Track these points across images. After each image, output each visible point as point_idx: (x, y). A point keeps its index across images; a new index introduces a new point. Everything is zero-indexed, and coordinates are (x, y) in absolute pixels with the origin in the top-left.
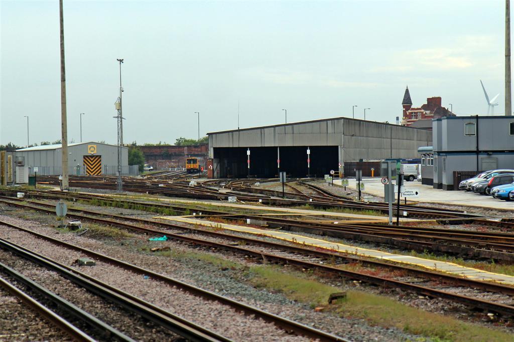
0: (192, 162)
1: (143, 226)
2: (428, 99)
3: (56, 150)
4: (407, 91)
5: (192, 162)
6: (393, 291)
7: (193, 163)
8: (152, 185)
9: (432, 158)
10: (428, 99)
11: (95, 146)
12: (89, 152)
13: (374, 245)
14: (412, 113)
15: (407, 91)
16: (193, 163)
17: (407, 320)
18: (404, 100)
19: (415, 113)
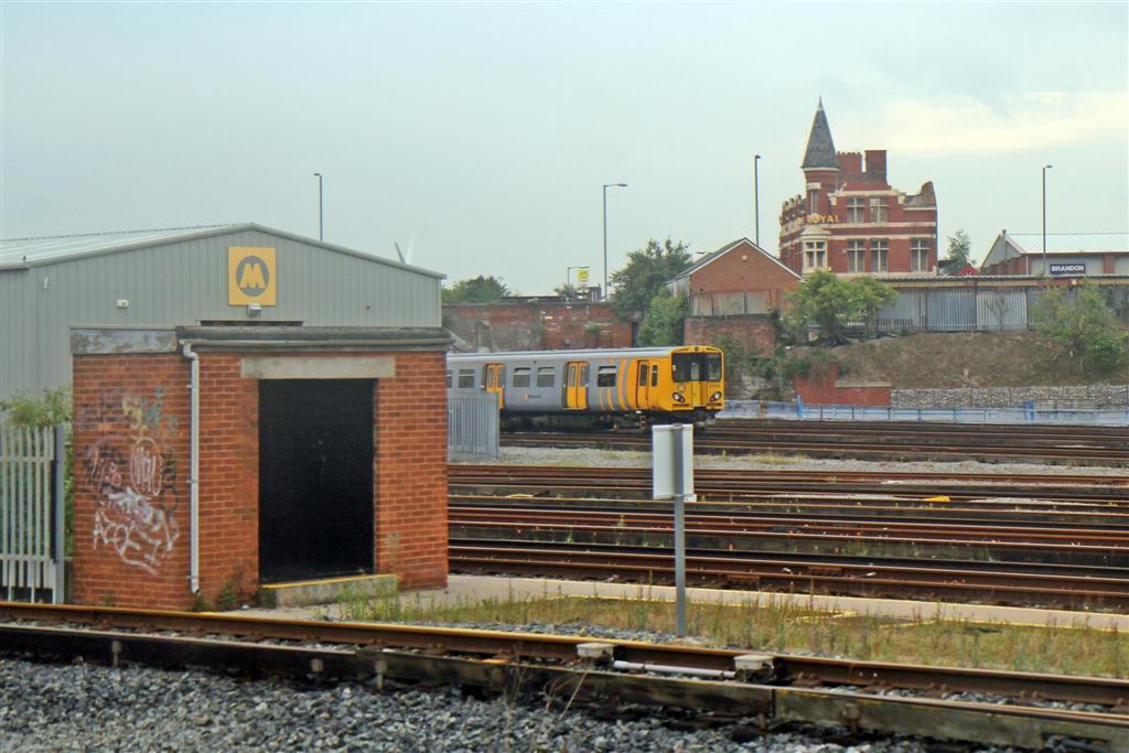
0: (695, 374)
1: (941, 664)
2: (491, 279)
3: (32, 271)
4: (821, 123)
5: (695, 374)
6: (681, 695)
7: (703, 377)
8: (398, 556)
9: (21, 557)
10: (491, 279)
11: (267, 254)
12: (237, 297)
13: (217, 677)
14: (850, 200)
15: (821, 123)
16: (703, 377)
17: (565, 739)
18: (809, 151)
19: (861, 200)
